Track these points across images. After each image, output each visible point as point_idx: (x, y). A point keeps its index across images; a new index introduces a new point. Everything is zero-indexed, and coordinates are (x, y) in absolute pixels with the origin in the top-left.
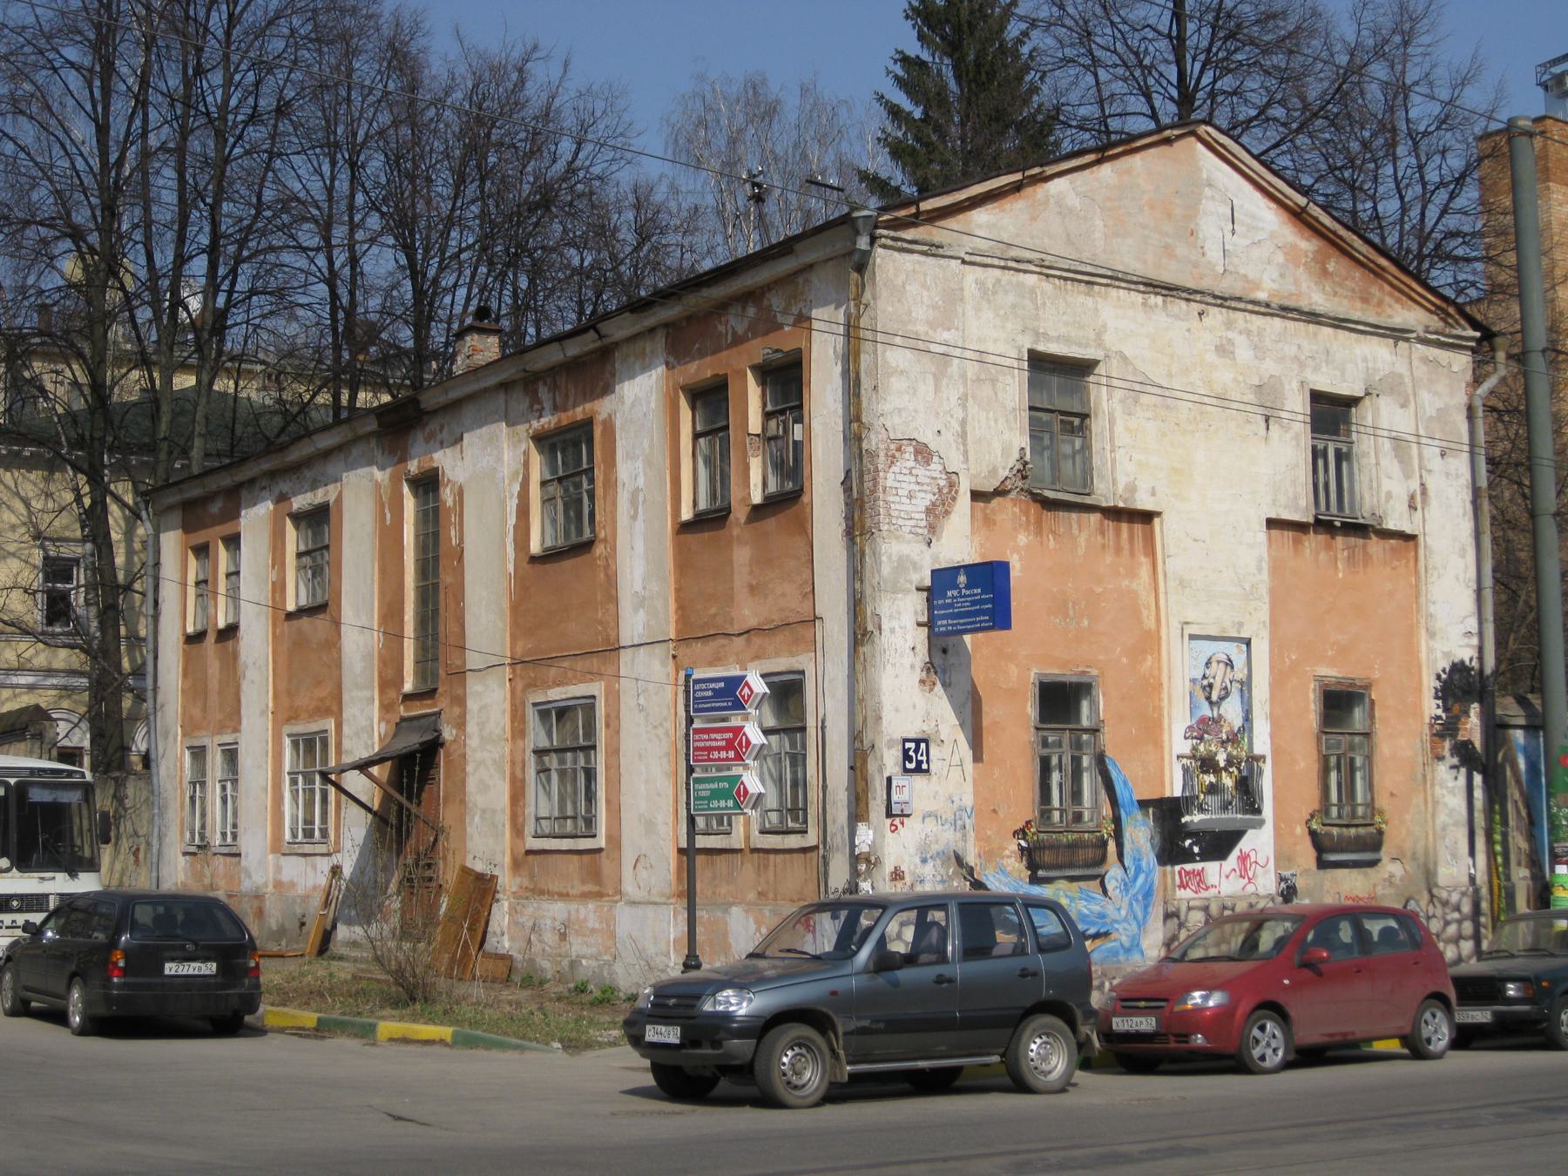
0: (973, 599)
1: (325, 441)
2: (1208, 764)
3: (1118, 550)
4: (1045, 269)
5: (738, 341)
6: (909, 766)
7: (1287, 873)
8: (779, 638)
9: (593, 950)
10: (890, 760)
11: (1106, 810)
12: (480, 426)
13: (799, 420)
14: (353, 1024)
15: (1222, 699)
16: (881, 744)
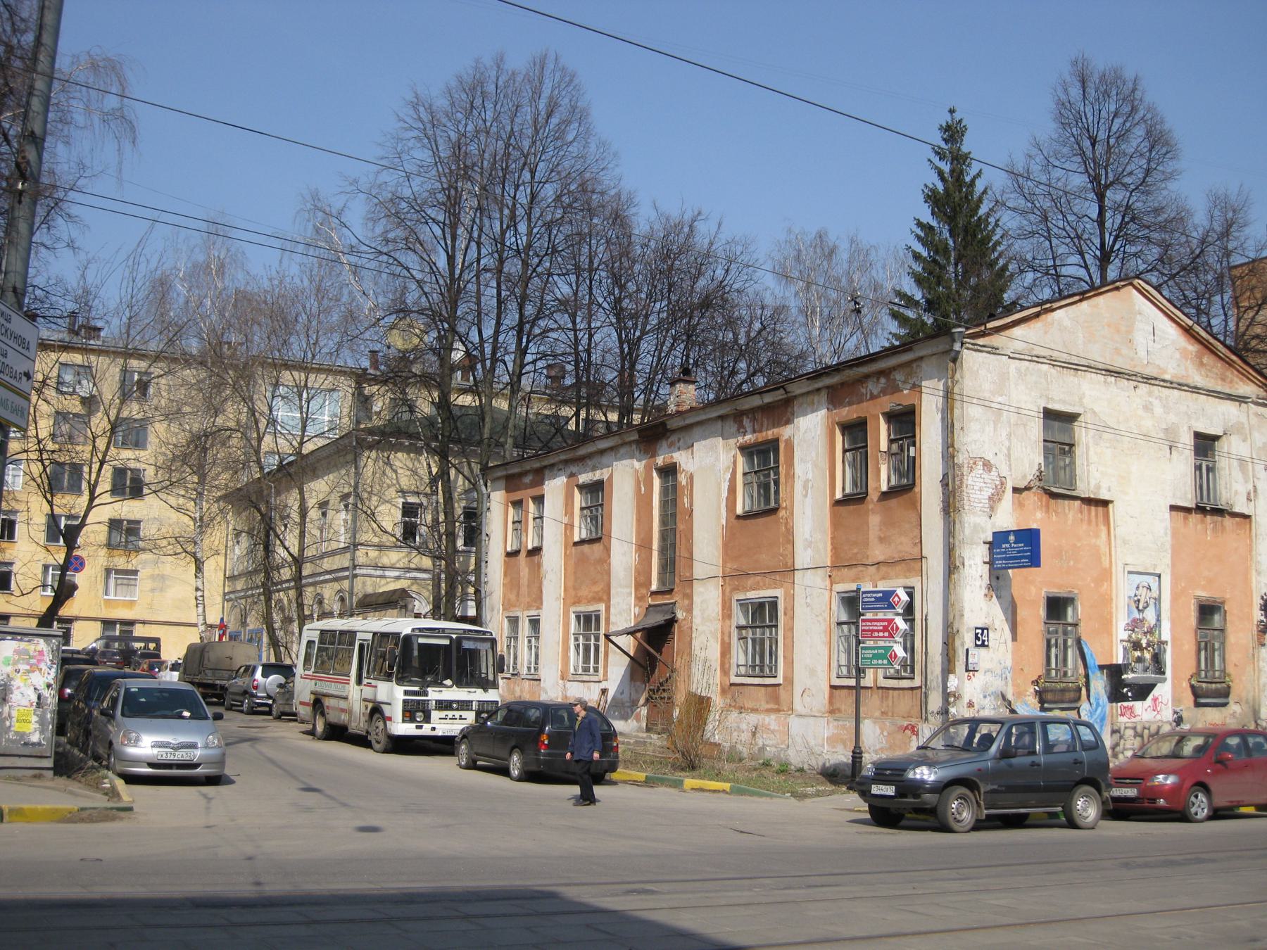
0: (1017, 549)
1: (602, 445)
2: (1137, 645)
3: (1090, 522)
4: (1053, 362)
5: (873, 397)
7: (1178, 709)
8: (898, 568)
9: (774, 742)
10: (968, 639)
11: (1081, 670)
12: (705, 439)
13: (914, 445)
14: (669, 780)
16: (963, 630)
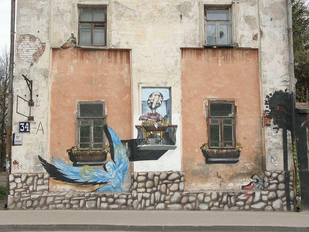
6: (21, 130)
15: (156, 107)
